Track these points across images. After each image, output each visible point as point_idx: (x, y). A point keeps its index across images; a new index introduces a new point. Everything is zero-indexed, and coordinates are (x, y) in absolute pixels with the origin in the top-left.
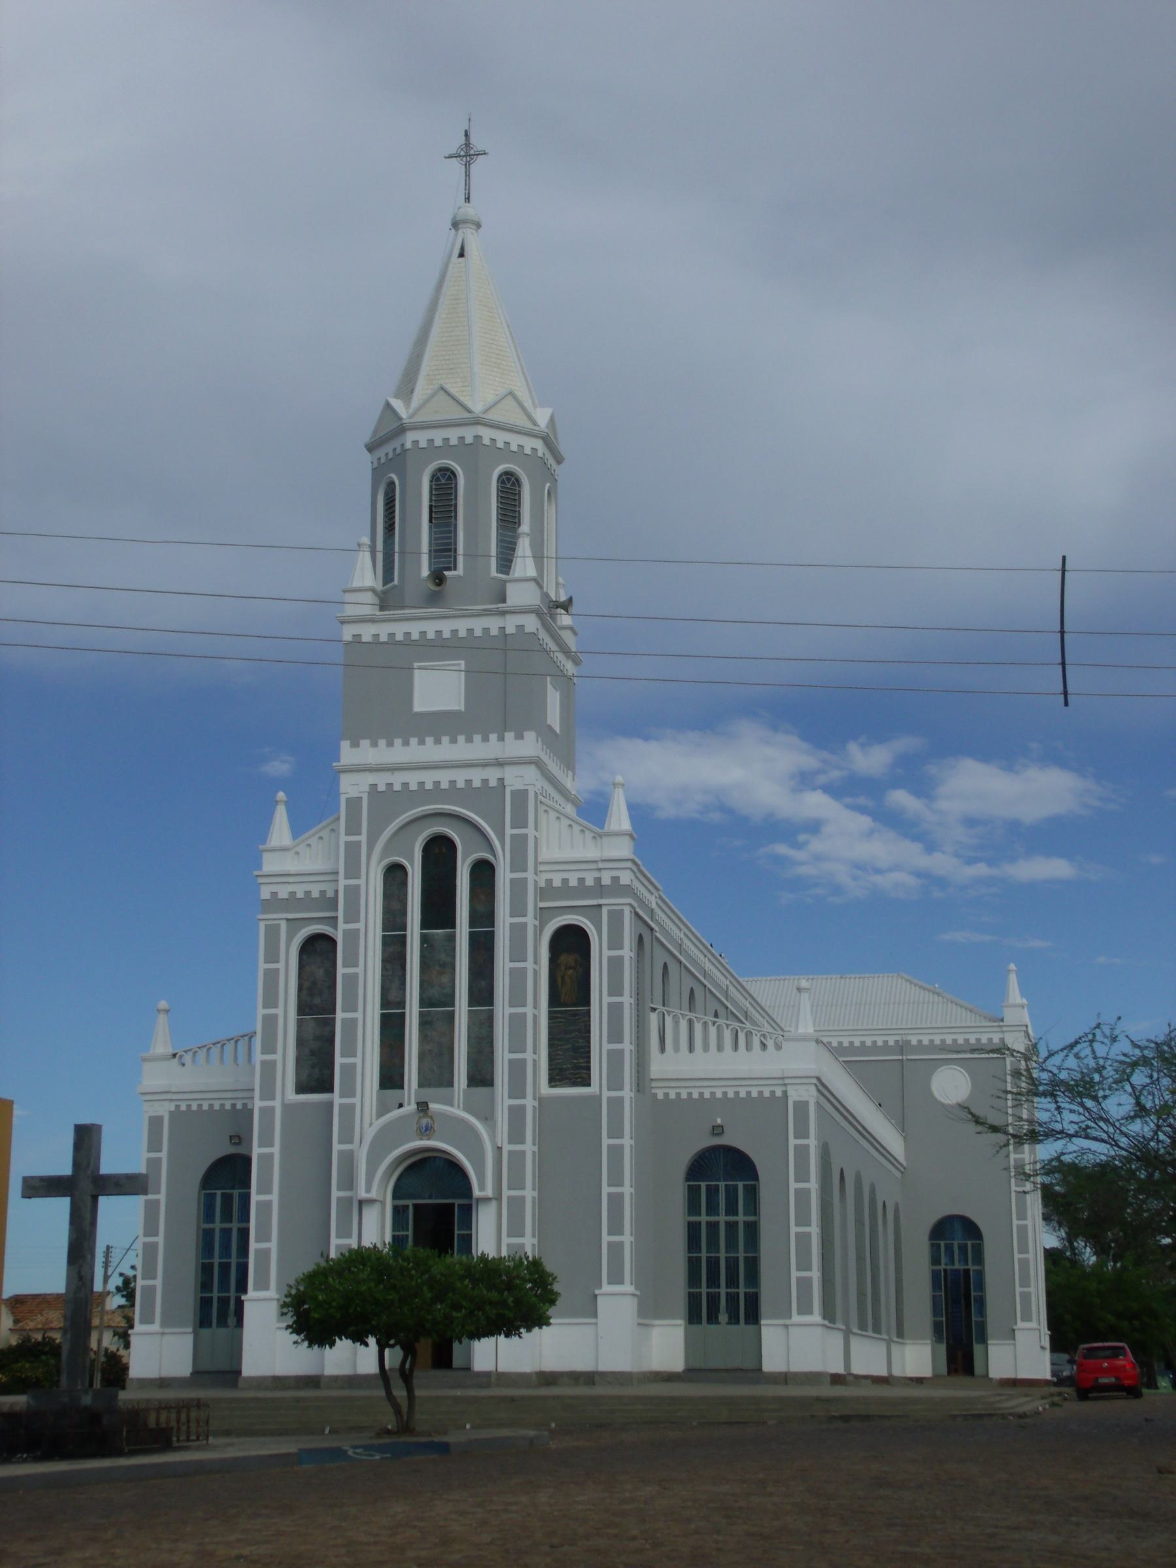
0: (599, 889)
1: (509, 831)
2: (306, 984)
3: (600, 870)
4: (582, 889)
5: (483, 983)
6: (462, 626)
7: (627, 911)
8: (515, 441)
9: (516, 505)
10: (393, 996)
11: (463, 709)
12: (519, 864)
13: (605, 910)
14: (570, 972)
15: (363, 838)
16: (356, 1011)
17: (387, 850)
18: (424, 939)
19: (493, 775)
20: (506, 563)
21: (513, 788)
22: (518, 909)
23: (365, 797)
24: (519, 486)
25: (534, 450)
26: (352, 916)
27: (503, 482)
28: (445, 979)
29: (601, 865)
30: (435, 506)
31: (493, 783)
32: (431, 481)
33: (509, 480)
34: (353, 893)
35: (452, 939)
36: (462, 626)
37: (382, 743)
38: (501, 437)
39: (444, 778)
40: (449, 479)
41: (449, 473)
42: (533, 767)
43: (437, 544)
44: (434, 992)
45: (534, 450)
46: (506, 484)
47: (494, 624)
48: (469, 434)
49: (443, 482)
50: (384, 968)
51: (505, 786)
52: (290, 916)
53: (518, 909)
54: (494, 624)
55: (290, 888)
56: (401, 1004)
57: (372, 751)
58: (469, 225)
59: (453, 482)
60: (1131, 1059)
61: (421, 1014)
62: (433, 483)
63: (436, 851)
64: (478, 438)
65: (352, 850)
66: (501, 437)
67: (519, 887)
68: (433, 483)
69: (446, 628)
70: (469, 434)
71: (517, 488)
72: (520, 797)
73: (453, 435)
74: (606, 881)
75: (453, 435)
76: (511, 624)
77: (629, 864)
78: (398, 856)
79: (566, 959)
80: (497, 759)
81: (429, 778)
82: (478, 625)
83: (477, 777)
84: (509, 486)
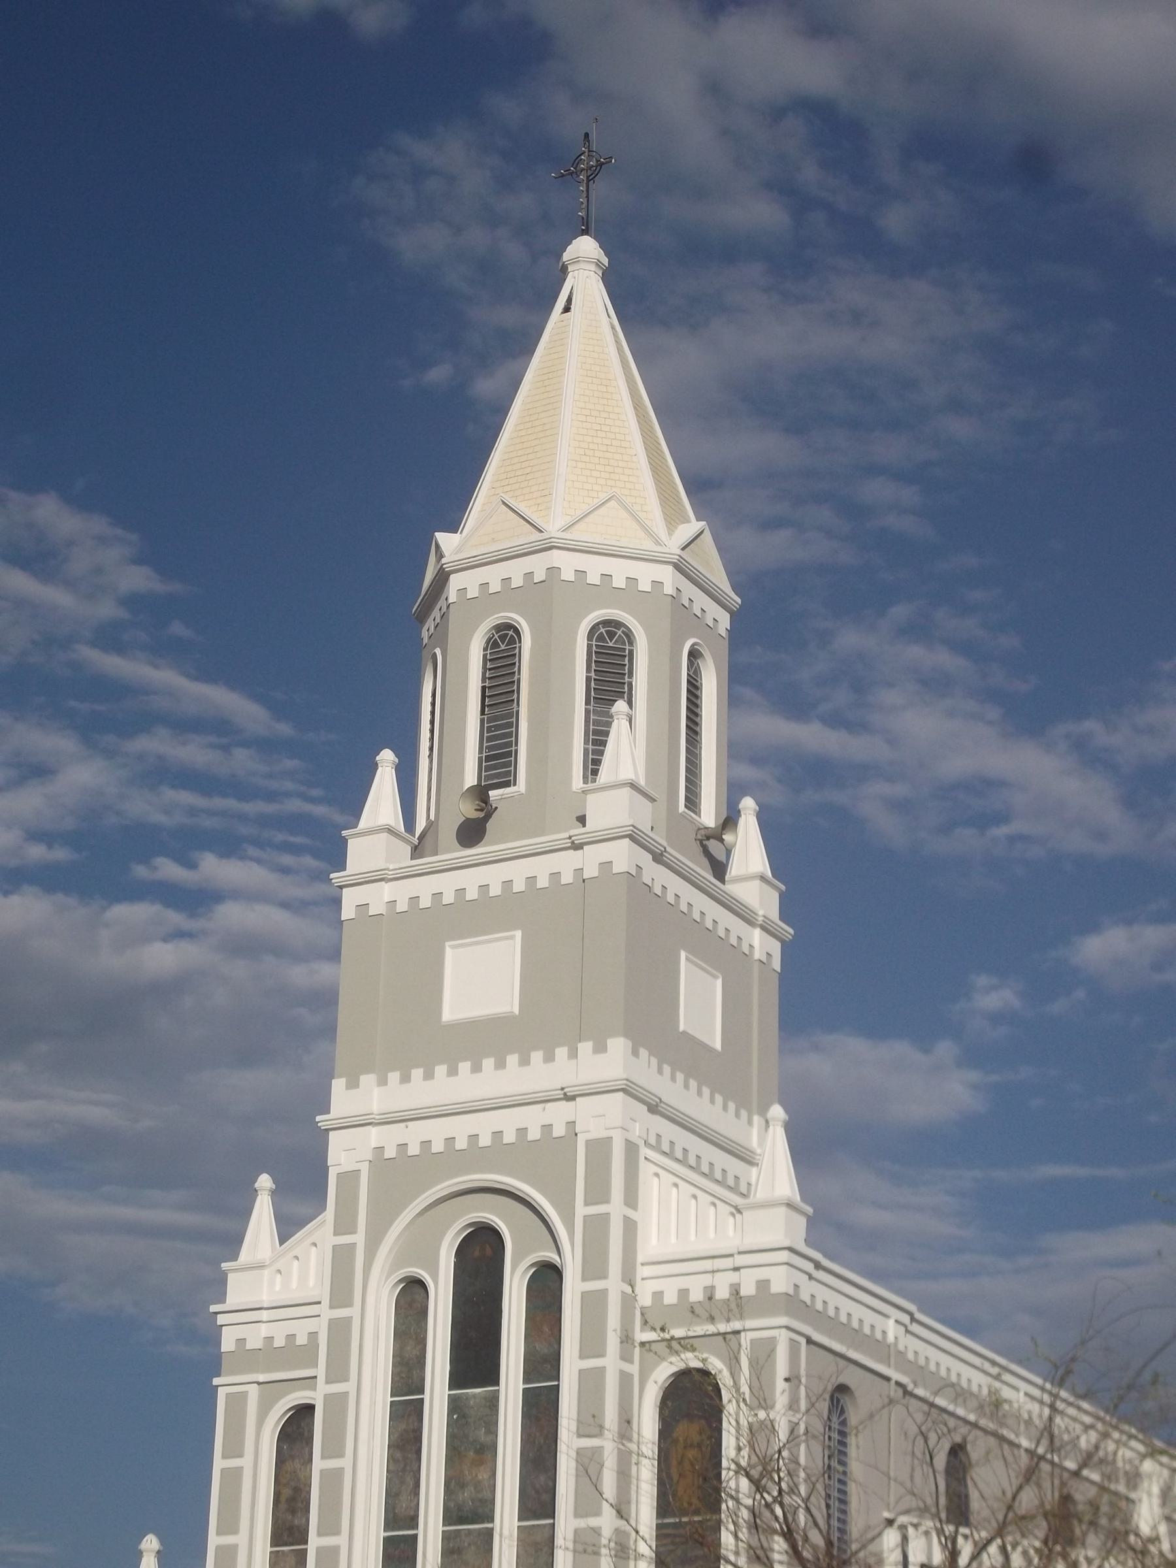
0: (738, 1304)
1: (581, 1210)
2: (287, 1492)
3: (736, 1269)
4: (708, 1309)
5: (542, 1478)
6: (517, 873)
7: (783, 1337)
8: (620, 571)
9: (625, 674)
10: (403, 1504)
11: (516, 1011)
12: (594, 1267)
13: (746, 1339)
14: (691, 1454)
15: (359, 1238)
16: (337, 1533)
17: (401, 1257)
18: (455, 1405)
19: (558, 1115)
20: (593, 766)
21: (590, 1136)
22: (592, 1345)
23: (365, 1169)
24: (631, 643)
25: (657, 584)
26: (338, 1372)
27: (601, 638)
28: (483, 1475)
29: (740, 1260)
30: (489, 688)
31: (559, 1131)
32: (485, 649)
33: (611, 635)
34: (340, 1331)
35: (492, 1403)
36: (517, 873)
37: (394, 1077)
38: (595, 568)
39: (484, 1126)
40: (512, 641)
41: (511, 633)
42: (621, 1094)
43: (489, 748)
44: (466, 1495)
45: (657, 584)
46: (608, 643)
47: (566, 864)
48: (538, 565)
49: (503, 647)
50: (391, 1459)
51: (576, 1135)
52: (262, 1378)
53: (592, 1345)
54: (566, 864)
55: (264, 1330)
56: (413, 1522)
57: (377, 1092)
58: (582, 265)
59: (518, 645)
60: (792, 1523)
61: (446, 1537)
62: (489, 652)
63: (477, 1254)
64: (553, 571)
65: (342, 1258)
66: (595, 568)
67: (594, 1304)
68: (489, 652)
69: (494, 877)
70: (538, 565)
71: (627, 647)
72: (599, 1149)
73: (515, 571)
74: (748, 1290)
75: (515, 571)
76: (590, 860)
77: (784, 1256)
78: (411, 1266)
79: (686, 1430)
80: (562, 1089)
81: (460, 1129)
82: (541, 869)
83: (533, 1120)
84: (611, 644)
